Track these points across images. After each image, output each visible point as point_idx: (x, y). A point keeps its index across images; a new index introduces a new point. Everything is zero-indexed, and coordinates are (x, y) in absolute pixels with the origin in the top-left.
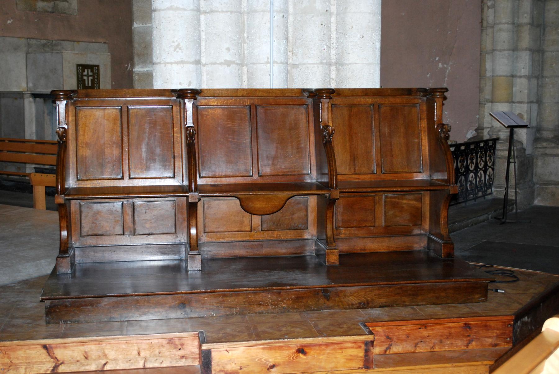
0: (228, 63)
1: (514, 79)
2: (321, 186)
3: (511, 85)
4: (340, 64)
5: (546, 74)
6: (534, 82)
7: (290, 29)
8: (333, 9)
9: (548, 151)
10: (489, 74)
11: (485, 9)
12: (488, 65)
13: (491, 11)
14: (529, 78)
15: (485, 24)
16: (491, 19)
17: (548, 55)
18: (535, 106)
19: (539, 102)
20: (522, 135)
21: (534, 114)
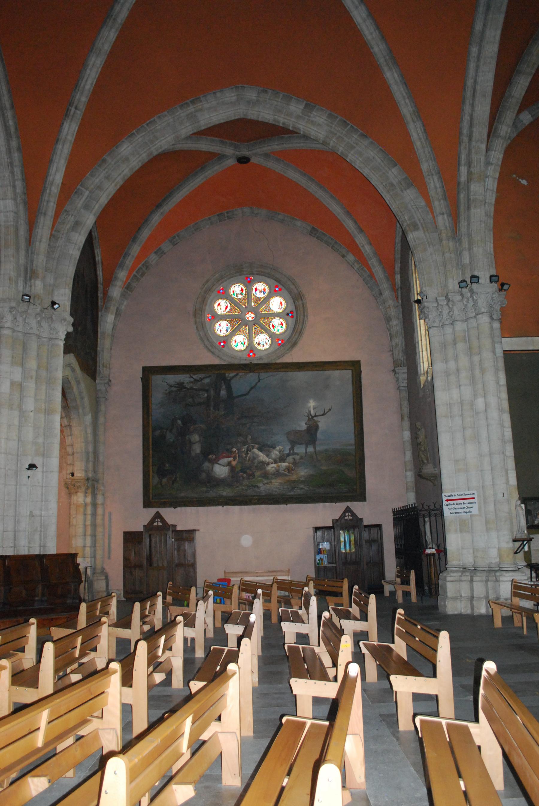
0: (11, 547)
1: (475, 596)
2: (315, 452)
3: (84, 550)
4: (44, 546)
5: (97, 545)
6: (93, 549)
7: (42, 538)
8: (42, 530)
9: (99, 578)
10: (74, 546)
11: (71, 518)
12: (73, 542)
13: (74, 520)
14: (91, 547)
15: (71, 524)
16: (74, 523)
17: (97, 537)
18: (93, 559)
19: (95, 557)
20: (89, 571)
21: (93, 563)
